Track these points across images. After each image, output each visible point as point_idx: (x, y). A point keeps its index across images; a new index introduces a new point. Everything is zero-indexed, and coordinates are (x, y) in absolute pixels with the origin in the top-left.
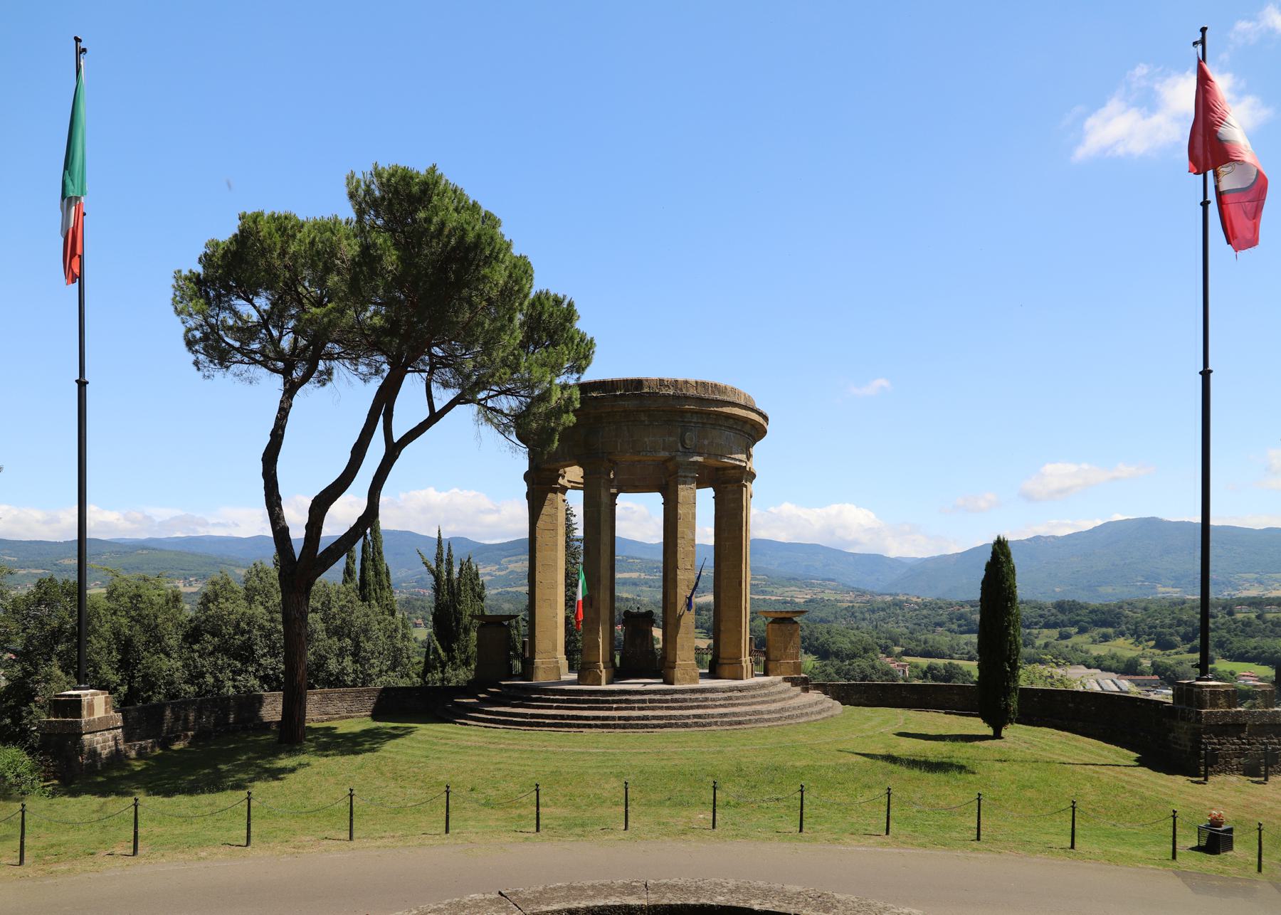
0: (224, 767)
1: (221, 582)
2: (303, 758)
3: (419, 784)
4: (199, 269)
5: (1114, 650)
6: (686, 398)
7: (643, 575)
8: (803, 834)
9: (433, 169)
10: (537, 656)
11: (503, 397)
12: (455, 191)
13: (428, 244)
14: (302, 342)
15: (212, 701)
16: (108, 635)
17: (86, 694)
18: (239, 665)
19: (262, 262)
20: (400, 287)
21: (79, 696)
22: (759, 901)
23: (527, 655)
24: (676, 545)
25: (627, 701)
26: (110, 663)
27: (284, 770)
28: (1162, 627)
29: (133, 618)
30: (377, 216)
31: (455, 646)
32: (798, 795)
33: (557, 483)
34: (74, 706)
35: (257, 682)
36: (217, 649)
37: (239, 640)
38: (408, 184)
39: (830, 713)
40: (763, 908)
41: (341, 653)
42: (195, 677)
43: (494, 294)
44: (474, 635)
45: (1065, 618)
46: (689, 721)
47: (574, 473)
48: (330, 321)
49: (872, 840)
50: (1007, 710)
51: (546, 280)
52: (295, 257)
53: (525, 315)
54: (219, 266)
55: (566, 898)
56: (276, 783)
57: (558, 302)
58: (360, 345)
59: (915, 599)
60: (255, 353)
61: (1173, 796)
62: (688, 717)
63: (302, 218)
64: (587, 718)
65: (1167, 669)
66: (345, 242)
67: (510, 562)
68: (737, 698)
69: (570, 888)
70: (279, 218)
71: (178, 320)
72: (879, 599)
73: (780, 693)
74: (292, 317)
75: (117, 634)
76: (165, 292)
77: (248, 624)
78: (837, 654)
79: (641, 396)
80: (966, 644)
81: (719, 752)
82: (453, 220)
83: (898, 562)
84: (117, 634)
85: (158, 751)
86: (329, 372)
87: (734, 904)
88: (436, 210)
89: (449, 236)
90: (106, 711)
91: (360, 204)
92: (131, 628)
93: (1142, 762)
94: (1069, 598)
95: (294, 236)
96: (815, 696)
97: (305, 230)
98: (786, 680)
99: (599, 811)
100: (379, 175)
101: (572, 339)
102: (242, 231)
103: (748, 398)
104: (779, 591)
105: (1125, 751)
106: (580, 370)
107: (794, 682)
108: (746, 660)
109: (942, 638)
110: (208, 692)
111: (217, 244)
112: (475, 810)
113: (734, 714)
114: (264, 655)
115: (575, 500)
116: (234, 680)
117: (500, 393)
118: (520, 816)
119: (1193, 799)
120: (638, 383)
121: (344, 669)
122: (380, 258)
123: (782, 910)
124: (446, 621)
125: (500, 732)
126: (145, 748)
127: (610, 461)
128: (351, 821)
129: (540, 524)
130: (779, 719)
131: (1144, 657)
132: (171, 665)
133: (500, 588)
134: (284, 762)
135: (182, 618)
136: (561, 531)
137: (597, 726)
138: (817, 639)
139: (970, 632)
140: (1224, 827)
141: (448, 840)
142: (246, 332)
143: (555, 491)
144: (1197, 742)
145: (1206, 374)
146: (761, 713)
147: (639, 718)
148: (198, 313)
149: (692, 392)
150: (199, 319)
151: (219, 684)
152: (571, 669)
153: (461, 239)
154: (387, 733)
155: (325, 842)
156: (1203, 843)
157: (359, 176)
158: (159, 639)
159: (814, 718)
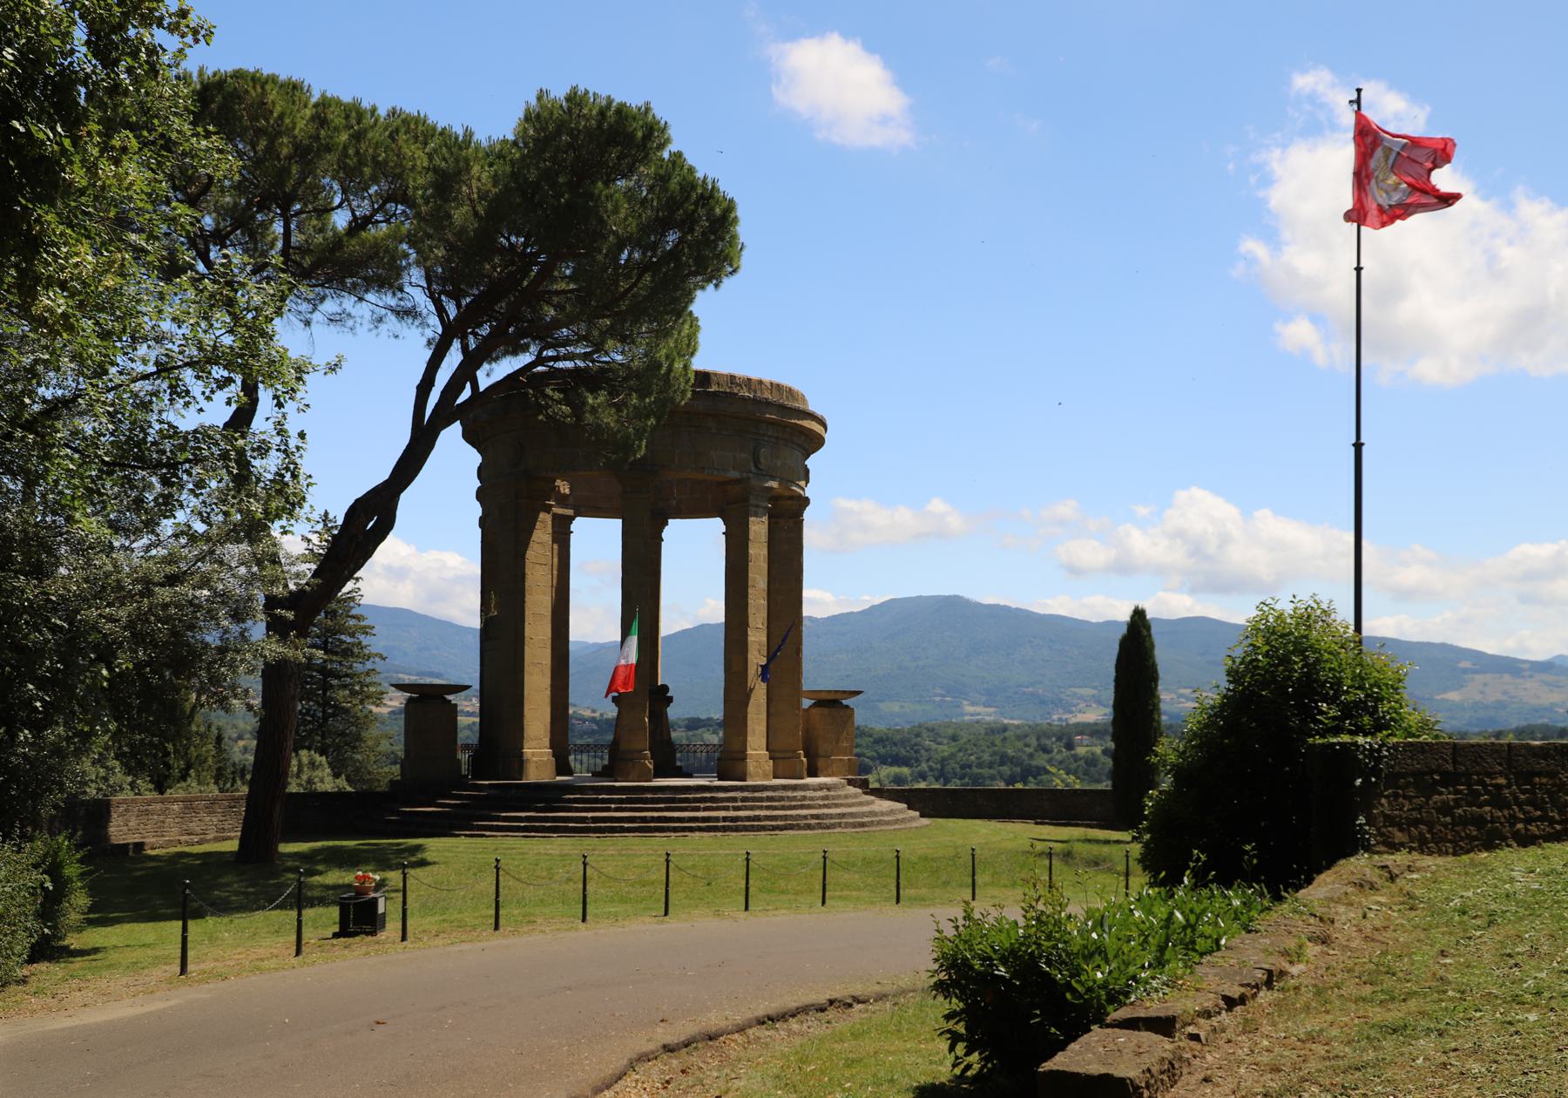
6: (767, 403)
10: (526, 745)
25: (713, 799)
28: (980, 765)
59: (588, 713)
62: (805, 817)
96: (887, 805)
98: (850, 782)
113: (852, 815)
145: (1358, 446)
147: (748, 819)
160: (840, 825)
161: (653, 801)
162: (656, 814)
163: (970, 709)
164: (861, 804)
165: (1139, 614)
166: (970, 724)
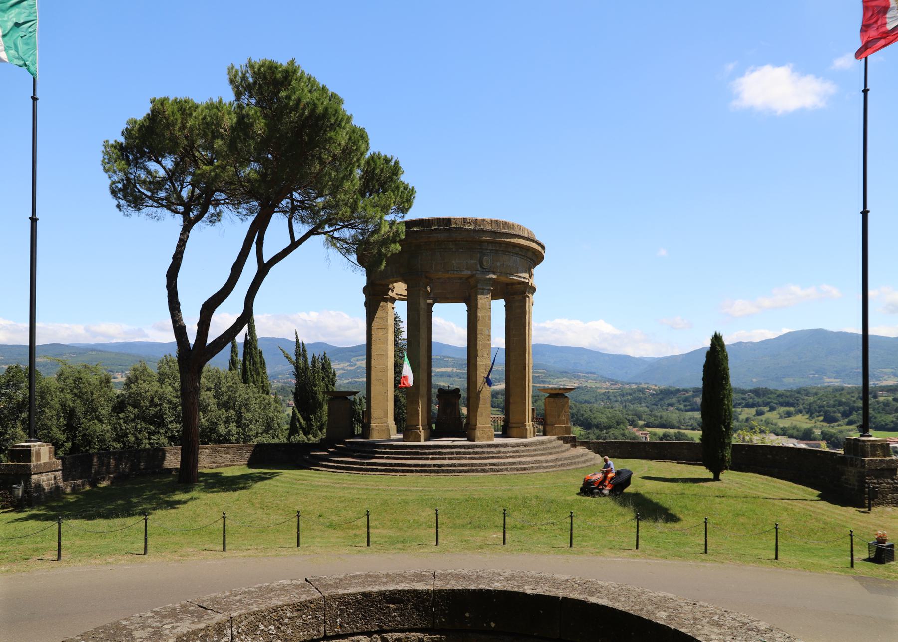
0: (135, 500)
1: (141, 369)
2: (194, 494)
3: (280, 512)
4: (122, 139)
5: (795, 423)
6: (484, 232)
7: (455, 370)
8: (573, 549)
9: (292, 62)
11: (345, 230)
12: (309, 79)
13: (288, 115)
14: (197, 191)
15: (132, 453)
16: (57, 406)
17: (35, 446)
18: (153, 428)
19: (167, 133)
20: (268, 151)
21: (30, 447)
22: (531, 587)
23: (365, 421)
24: (476, 339)
25: (439, 453)
26: (58, 427)
27: (179, 502)
28: (828, 406)
29: (76, 394)
30: (251, 97)
31: (312, 416)
32: (569, 520)
33: (387, 295)
34: (26, 454)
35: (166, 441)
36: (137, 417)
37: (153, 410)
38: (274, 73)
39: (592, 463)
40: (535, 592)
41: (228, 421)
42: (120, 437)
43: (338, 151)
44: (326, 407)
45: (760, 400)
46: (486, 468)
47: (400, 288)
48: (216, 174)
49: (625, 553)
50: (723, 459)
51: (379, 144)
52: (191, 129)
53: (362, 170)
54: (136, 138)
55: (363, 584)
56: (173, 511)
57: (387, 161)
58: (239, 193)
59: (653, 387)
60: (162, 199)
61: (846, 522)
62: (486, 465)
63: (197, 101)
64: (409, 466)
65: (831, 436)
66: (227, 116)
67: (358, 360)
68: (523, 451)
69: (368, 576)
70: (180, 102)
71: (106, 175)
72: (627, 386)
73: (555, 448)
74: (190, 173)
75: (63, 405)
76: (98, 155)
77: (160, 399)
78: (598, 426)
79: (450, 230)
80: (690, 419)
81: (509, 490)
82: (307, 98)
83: (641, 361)
84: (63, 405)
85: (88, 488)
86: (218, 215)
87: (509, 589)
88: (294, 90)
89: (304, 109)
90: (50, 459)
91: (237, 87)
92: (74, 402)
93: (822, 498)
94: (763, 386)
95: (191, 114)
96: (581, 450)
97: (199, 110)
98: (559, 439)
99: (416, 532)
100: (252, 66)
101: (397, 187)
102: (152, 111)
103: (530, 233)
104: (556, 380)
105: (810, 489)
106: (404, 210)
107: (565, 440)
108: (529, 424)
109: (673, 414)
110: (130, 447)
111: (135, 122)
112: (321, 530)
113: (520, 463)
114: (171, 422)
115: (401, 308)
116: (150, 439)
117: (343, 227)
118: (355, 535)
119: (861, 524)
120: (448, 221)
121: (230, 431)
122: (252, 124)
123: (551, 594)
124: (305, 396)
125: (344, 476)
126: (79, 486)
127: (426, 278)
128: (224, 537)
129: (374, 324)
130: (555, 467)
131: (815, 427)
132: (103, 428)
133: (347, 376)
134: (179, 496)
135: (111, 394)
136: (391, 330)
137: (416, 471)
138: (583, 415)
139: (693, 410)
140: (887, 544)
141: (300, 551)
142: (157, 185)
143: (386, 300)
144: (862, 482)
145: (865, 213)
146: (541, 462)
147: (448, 466)
148: (120, 170)
149: (488, 228)
150: (121, 175)
151: (138, 441)
152: (398, 432)
153: (313, 111)
154: (260, 477)
155: (204, 552)
156: (872, 556)
157: (237, 67)
158: (94, 410)
159: (580, 466)
161: (407, 454)
163: (828, 380)
165: (717, 340)
166: (826, 387)
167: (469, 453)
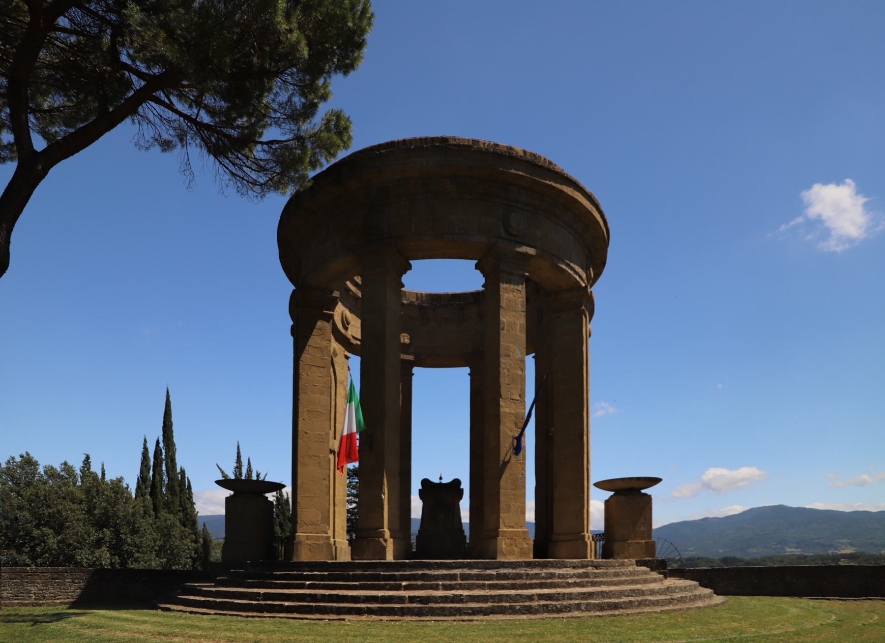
41: (99, 543)
46: (535, 604)
62: (530, 598)
113: (603, 594)
137: (370, 612)
147: (445, 599)
160: (578, 607)
162: (327, 592)
163: (789, 550)
164: (646, 581)
166: (789, 556)
167: (490, 577)
